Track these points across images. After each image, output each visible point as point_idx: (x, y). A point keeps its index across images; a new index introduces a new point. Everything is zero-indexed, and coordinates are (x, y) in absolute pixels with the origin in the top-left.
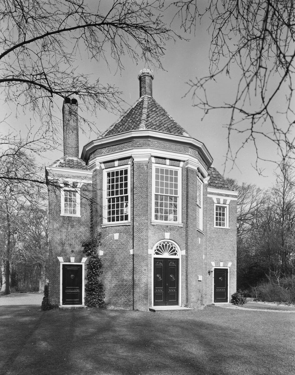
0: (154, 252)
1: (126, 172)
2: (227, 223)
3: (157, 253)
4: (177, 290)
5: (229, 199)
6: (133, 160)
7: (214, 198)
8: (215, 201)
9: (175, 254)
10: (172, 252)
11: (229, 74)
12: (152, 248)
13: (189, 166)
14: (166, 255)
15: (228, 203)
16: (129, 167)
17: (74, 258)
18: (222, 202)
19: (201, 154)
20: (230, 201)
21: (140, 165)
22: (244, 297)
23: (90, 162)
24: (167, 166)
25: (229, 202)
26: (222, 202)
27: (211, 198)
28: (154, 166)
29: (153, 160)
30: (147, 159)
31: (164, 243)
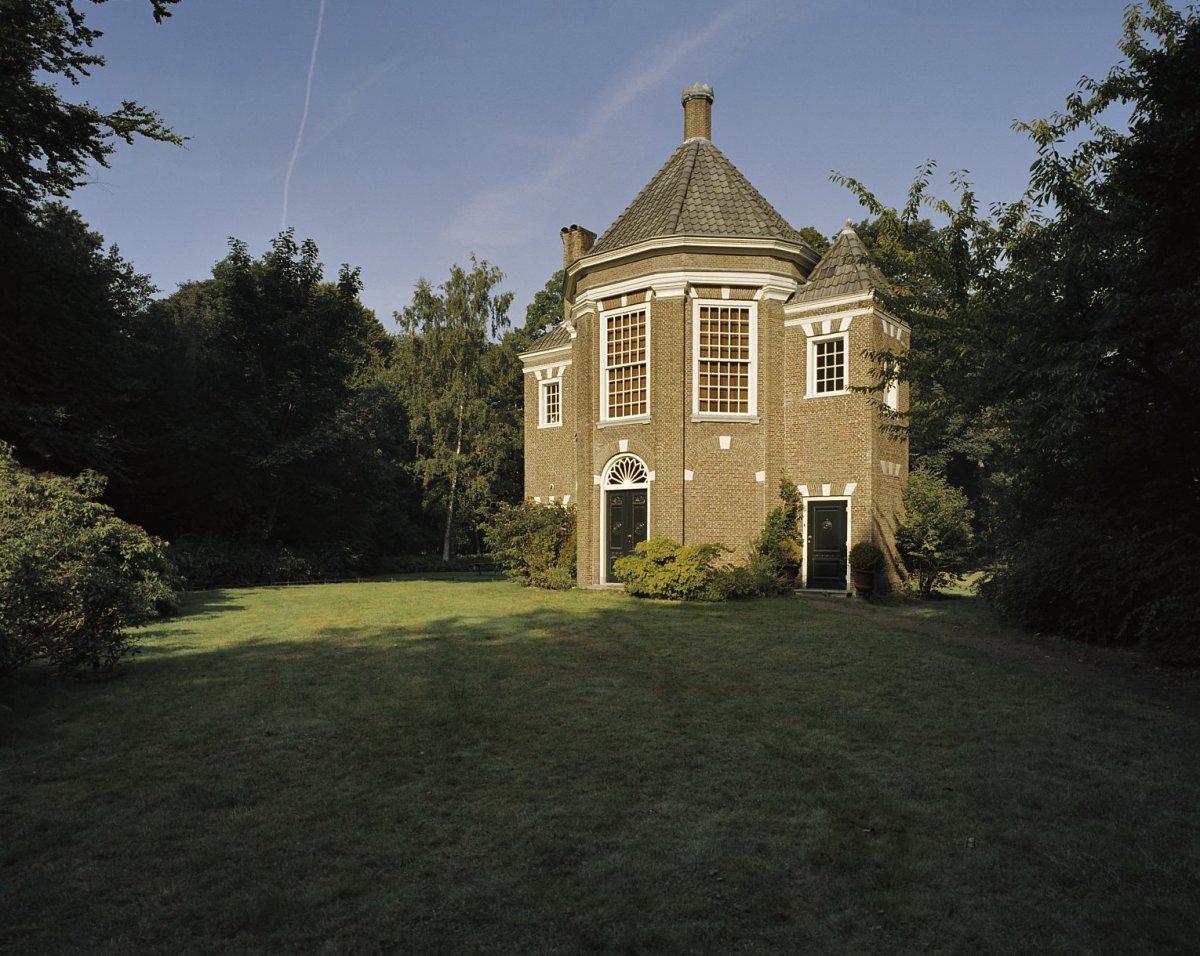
0: (607, 480)
1: (642, 314)
2: (813, 354)
3: (612, 482)
4: (646, 525)
5: (846, 319)
6: (655, 294)
7: (806, 325)
8: (809, 331)
9: (643, 480)
10: (637, 477)
11: (867, 221)
12: (600, 474)
13: (659, 295)
14: (628, 484)
15: (844, 326)
16: (647, 307)
17: (829, 486)
18: (826, 328)
19: (701, 251)
20: (829, 322)
21: (668, 303)
22: (904, 249)
23: (577, 299)
24: (725, 300)
25: (849, 323)
26: (826, 328)
27: (798, 329)
28: (697, 305)
29: (693, 293)
30: (682, 293)
31: (624, 460)
